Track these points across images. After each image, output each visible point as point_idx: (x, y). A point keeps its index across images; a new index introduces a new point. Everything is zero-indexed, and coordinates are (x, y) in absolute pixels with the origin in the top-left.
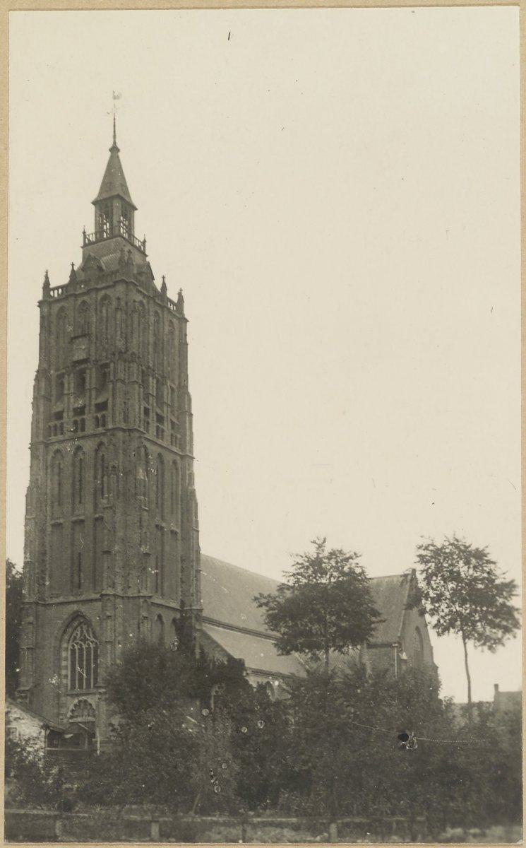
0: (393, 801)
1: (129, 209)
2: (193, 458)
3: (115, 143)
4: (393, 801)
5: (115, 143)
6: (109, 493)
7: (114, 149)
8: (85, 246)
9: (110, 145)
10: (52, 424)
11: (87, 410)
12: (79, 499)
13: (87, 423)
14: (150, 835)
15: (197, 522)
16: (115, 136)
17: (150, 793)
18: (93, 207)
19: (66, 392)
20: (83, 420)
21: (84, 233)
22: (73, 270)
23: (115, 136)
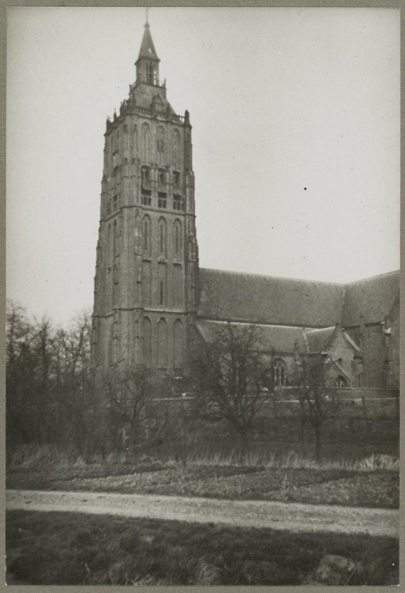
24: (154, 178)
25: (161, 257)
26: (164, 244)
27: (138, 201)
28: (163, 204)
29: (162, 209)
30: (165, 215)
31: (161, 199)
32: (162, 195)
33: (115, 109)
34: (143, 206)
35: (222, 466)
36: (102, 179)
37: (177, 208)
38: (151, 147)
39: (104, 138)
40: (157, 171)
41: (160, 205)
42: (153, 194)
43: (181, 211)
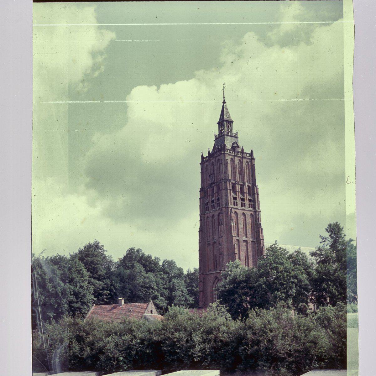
0: (217, 352)
1: (230, 122)
2: (260, 212)
3: (224, 100)
4: (217, 352)
5: (224, 100)
6: (221, 232)
7: (224, 102)
8: (216, 139)
9: (223, 101)
10: (205, 207)
11: (209, 203)
12: (33, 281)
13: (215, 206)
14: (345, 341)
15: (262, 236)
16: (224, 98)
17: (285, 333)
18: (218, 125)
19: (209, 195)
20: (214, 205)
21: (215, 135)
22: (209, 152)
23: (224, 98)
24: (246, 191)
25: (244, 238)
26: (242, 226)
27: (231, 204)
28: (243, 205)
29: (243, 208)
30: (245, 212)
31: (242, 202)
32: (243, 200)
33: (209, 149)
34: (234, 207)
35: (156, 86)
36: (170, 84)
37: (251, 207)
38: (235, 172)
39: (200, 166)
40: (239, 185)
41: (242, 206)
42: (238, 199)
43: (214, 187)
